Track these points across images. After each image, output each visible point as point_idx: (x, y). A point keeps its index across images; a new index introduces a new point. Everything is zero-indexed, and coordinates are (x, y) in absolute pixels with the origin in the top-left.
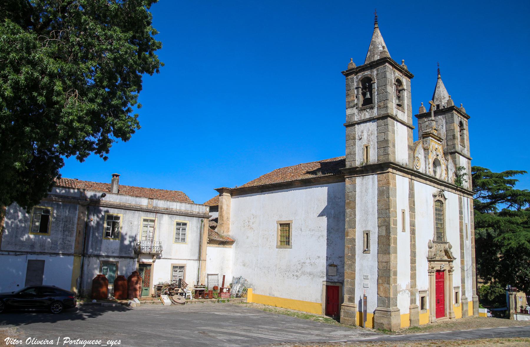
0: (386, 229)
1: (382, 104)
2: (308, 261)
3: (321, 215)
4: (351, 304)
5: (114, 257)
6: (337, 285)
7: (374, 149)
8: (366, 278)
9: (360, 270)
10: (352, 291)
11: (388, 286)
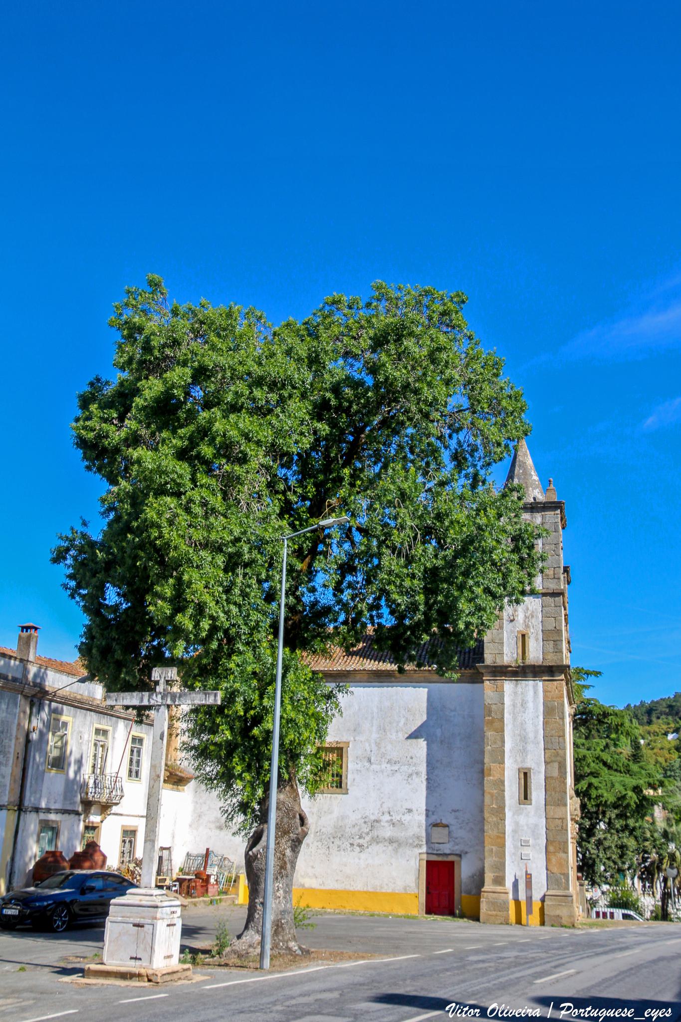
0: (560, 768)
1: (552, 572)
2: (387, 817)
3: (414, 736)
4: (499, 888)
5: (57, 811)
6: (450, 858)
7: (537, 640)
8: (525, 844)
9: (515, 831)
10: (501, 867)
11: (564, 855)
